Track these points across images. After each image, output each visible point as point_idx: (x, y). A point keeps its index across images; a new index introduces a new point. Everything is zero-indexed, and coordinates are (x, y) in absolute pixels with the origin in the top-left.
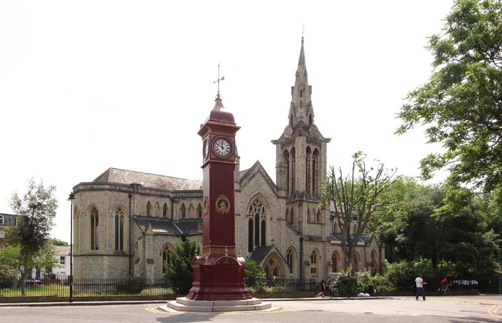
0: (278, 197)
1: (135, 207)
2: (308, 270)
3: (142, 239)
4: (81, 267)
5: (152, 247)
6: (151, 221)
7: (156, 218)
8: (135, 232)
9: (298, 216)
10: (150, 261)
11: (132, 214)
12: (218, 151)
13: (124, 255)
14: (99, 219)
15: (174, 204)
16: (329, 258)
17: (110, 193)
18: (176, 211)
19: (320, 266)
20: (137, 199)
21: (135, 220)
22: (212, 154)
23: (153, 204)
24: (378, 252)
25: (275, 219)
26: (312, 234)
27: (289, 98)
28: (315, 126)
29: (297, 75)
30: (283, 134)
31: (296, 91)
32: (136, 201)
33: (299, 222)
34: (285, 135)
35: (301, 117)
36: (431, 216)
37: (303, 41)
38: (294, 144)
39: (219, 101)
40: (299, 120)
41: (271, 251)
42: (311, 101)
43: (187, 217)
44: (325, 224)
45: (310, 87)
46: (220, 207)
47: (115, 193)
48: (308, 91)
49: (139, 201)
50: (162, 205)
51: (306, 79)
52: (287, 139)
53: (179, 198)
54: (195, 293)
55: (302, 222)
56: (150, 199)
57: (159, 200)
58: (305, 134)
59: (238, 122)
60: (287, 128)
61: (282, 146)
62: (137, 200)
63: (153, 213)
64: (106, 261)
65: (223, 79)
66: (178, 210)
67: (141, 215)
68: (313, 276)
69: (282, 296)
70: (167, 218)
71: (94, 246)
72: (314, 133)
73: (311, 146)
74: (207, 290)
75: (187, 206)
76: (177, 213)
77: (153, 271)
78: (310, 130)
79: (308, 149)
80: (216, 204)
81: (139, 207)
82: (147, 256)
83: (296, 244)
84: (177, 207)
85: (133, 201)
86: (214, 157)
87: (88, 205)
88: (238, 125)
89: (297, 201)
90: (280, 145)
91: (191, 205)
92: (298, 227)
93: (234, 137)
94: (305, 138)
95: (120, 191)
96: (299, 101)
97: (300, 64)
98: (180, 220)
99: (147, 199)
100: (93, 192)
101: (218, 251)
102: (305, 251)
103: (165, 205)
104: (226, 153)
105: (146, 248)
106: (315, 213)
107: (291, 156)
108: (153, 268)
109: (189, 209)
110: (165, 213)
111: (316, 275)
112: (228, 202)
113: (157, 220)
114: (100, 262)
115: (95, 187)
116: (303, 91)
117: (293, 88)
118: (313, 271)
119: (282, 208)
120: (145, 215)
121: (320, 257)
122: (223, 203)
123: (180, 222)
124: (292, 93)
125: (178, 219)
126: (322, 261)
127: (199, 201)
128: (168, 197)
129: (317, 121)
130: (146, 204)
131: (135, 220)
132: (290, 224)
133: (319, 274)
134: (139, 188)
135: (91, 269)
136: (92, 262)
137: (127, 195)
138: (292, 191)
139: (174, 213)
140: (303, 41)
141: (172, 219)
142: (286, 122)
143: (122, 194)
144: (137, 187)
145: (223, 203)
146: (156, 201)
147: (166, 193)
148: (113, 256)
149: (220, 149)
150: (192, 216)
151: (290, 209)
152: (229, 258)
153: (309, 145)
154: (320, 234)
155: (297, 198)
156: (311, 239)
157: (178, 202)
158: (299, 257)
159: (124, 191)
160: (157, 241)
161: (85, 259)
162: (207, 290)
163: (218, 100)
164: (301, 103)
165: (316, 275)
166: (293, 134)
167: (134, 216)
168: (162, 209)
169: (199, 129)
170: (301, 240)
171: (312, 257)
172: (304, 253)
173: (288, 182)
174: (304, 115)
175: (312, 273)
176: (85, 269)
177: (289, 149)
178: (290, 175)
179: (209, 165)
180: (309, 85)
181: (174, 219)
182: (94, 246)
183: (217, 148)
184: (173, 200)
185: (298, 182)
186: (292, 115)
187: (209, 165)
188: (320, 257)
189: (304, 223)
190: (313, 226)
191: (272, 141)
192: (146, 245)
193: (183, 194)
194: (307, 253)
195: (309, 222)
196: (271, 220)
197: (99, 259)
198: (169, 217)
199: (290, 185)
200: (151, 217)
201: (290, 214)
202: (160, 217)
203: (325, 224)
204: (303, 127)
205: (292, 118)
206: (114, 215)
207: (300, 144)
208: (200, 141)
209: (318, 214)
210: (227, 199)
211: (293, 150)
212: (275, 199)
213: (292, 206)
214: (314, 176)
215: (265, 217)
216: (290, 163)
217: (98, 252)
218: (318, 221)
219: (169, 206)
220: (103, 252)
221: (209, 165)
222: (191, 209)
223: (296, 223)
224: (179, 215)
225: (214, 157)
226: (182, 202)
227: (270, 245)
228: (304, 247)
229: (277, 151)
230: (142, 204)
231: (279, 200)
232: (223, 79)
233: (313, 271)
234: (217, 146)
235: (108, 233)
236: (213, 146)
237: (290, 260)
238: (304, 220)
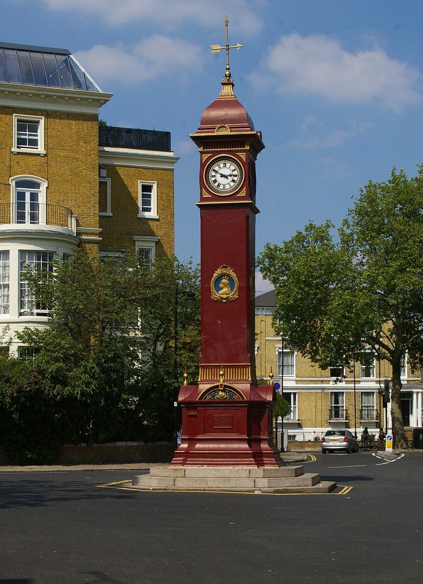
12: (216, 184)
22: (203, 190)
36: (92, 393)
46: (218, 289)
65: (228, 22)
80: (212, 285)
86: (207, 195)
104: (228, 165)
112: (236, 279)
117: (412, 414)
162: (253, 437)
183: (213, 179)
210: (233, 275)
225: (207, 195)
232: (228, 22)
234: (213, 174)
236: (220, 192)
237: (28, 236)
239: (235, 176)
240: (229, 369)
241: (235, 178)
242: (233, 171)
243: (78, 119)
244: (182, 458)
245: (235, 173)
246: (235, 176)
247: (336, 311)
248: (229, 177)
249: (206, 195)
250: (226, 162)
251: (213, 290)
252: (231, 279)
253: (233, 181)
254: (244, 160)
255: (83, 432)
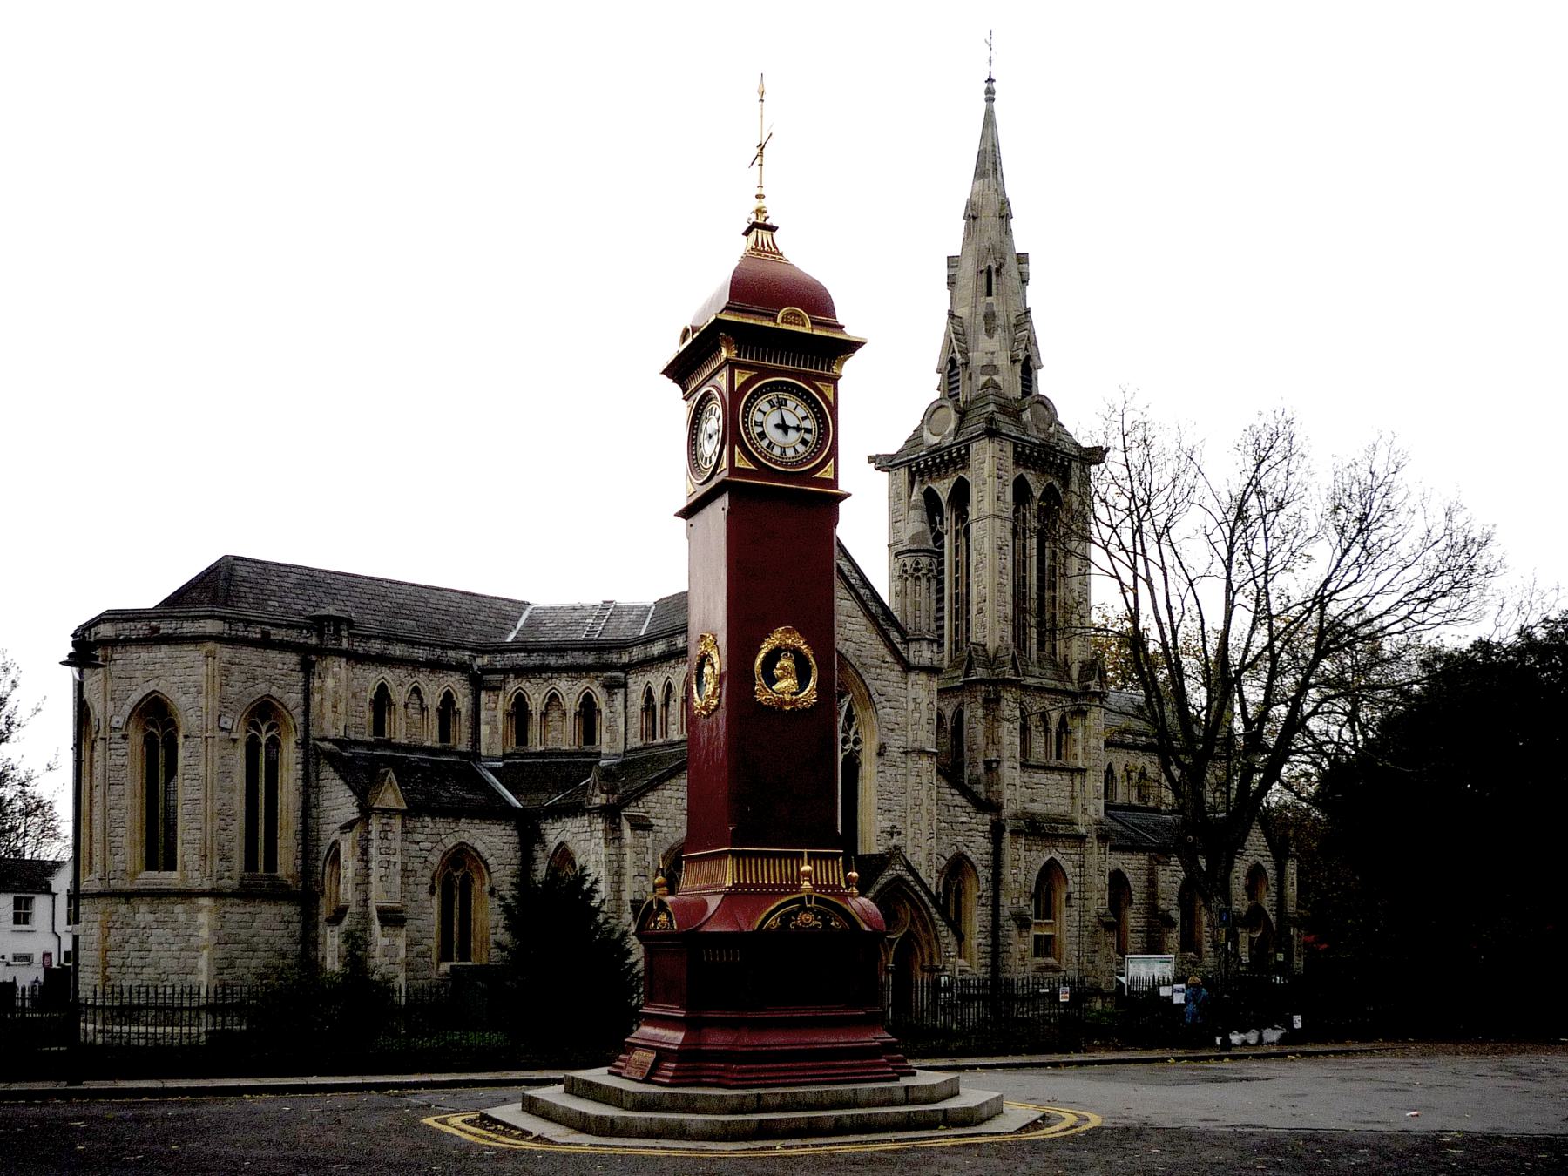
0: (907, 668)
1: (328, 705)
2: (1019, 945)
3: (357, 830)
4: (105, 941)
5: (397, 858)
6: (390, 762)
7: (409, 748)
8: (326, 803)
9: (980, 740)
10: (392, 918)
11: (314, 733)
13: (276, 893)
14: (181, 753)
15: (483, 695)
16: (1098, 901)
17: (226, 653)
18: (492, 723)
19: (1067, 927)
20: (336, 677)
21: (331, 758)
23: (399, 695)
24: (1270, 870)
25: (894, 753)
26: (1036, 808)
27: (942, 300)
28: (1044, 402)
29: (972, 217)
30: (919, 430)
31: (968, 271)
32: (330, 682)
33: (988, 764)
34: (926, 434)
35: (991, 368)
37: (990, 95)
38: (965, 466)
39: (764, 235)
40: (983, 379)
41: (889, 874)
42: (1028, 311)
43: (535, 745)
44: (1085, 771)
45: (1022, 259)
46: (771, 680)
47: (249, 655)
48: (1016, 274)
49: (344, 682)
50: (433, 699)
51: (1007, 231)
52: (936, 450)
53: (505, 672)
54: (663, 1055)
55: (998, 762)
56: (389, 675)
57: (421, 678)
58: (1007, 426)
59: (851, 319)
60: (933, 410)
61: (912, 476)
62: (335, 676)
63: (398, 731)
64: (205, 916)
66: (500, 715)
67: (352, 737)
68: (1040, 968)
69: (953, 1046)
70: (451, 751)
71: (159, 849)
72: (1042, 426)
73: (1030, 477)
74: (717, 1040)
75: (536, 702)
76: (493, 732)
77: (402, 954)
78: (1026, 416)
79: (1021, 491)
81: (341, 708)
82: (378, 895)
83: (978, 849)
84: (495, 708)
85: (317, 683)
87: (136, 696)
88: (852, 332)
89: (981, 681)
90: (903, 473)
91: (553, 698)
92: (983, 779)
93: (834, 380)
94: (1009, 448)
95: (265, 643)
96: (981, 310)
97: (980, 173)
98: (505, 756)
99: (372, 677)
100: (155, 648)
101: (764, 875)
102: (1008, 874)
103: (448, 700)
104: (801, 448)
105: (373, 865)
106: (1047, 730)
107: (948, 514)
108: (401, 942)
109: (544, 715)
110: (445, 734)
111: (1051, 961)
113: (414, 757)
114: (182, 918)
115: (166, 628)
116: (998, 270)
117: (952, 262)
118: (1044, 946)
119: (923, 707)
120: (368, 737)
121: (1069, 897)
122: (786, 662)
123: (506, 765)
124: (952, 282)
125: (499, 753)
126: (1074, 911)
127: (585, 683)
128: (461, 667)
129: (1046, 384)
130: (370, 695)
131: (331, 758)
132: (952, 769)
133: (1064, 960)
134: (344, 633)
135: (143, 947)
136: (151, 917)
137: (292, 659)
138: (957, 646)
139: (485, 730)
140: (990, 95)
141: (475, 754)
142: (929, 388)
143: (274, 655)
144: (337, 632)
145: (786, 662)
146: (409, 682)
147: (451, 653)
148: (234, 894)
149: (775, 435)
150: (555, 740)
151: (949, 712)
152: (818, 900)
153: (1021, 471)
154: (1068, 809)
155: (980, 672)
156: (1037, 829)
157: (499, 689)
158: (989, 893)
159: (283, 646)
160: (417, 837)
161: (123, 909)
162: (717, 1040)
163: (760, 225)
164: (990, 317)
165: (1051, 961)
166: (958, 429)
167: (324, 739)
168: (433, 713)
169: (673, 348)
170: (996, 832)
171: (1035, 896)
172: (1010, 878)
173: (941, 609)
174: (1002, 360)
175: (69, 923)
176: (120, 947)
177: (943, 488)
178: (946, 585)
179: (726, 497)
180: (1019, 250)
181: (484, 752)
182: (159, 849)
183: (758, 430)
184: (478, 683)
185: (980, 611)
186: (952, 361)
187: (723, 502)
188: (1069, 897)
189: (1006, 764)
190: (1040, 777)
191: (872, 459)
192: (372, 850)
193: (519, 658)
194: (1021, 878)
195: (1025, 766)
196: (880, 754)
197: (179, 909)
198: (464, 746)
199: (947, 622)
200: (388, 744)
201: (953, 733)
202: (428, 744)
203: (1085, 771)
204: (999, 405)
205: (952, 370)
206: (240, 735)
207: (988, 468)
208: (673, 403)
209: (1059, 735)
211: (961, 493)
212: (893, 674)
213: (955, 702)
214: (1041, 588)
215: (856, 742)
216: (946, 538)
217: (171, 879)
218: (1059, 757)
219: (463, 703)
220: (197, 881)
221: (726, 497)
222: (555, 715)
223: (974, 764)
224: (505, 737)
226: (513, 685)
227: (876, 849)
228: (1007, 857)
229: (894, 497)
230: (354, 695)
231: (912, 677)
233: (1044, 946)
235: (217, 806)
238: (1006, 754)
239: (808, 431)
240: (771, 861)
241: (808, 437)
242: (804, 418)
243: (888, 1124)
244: (674, 1065)
245: (807, 424)
246: (808, 431)
247: (1351, 644)
248: (792, 433)
249: (741, 463)
250: (786, 396)
251: (760, 683)
252: (797, 653)
253: (804, 442)
254: (817, 475)
255: (13, 1016)
